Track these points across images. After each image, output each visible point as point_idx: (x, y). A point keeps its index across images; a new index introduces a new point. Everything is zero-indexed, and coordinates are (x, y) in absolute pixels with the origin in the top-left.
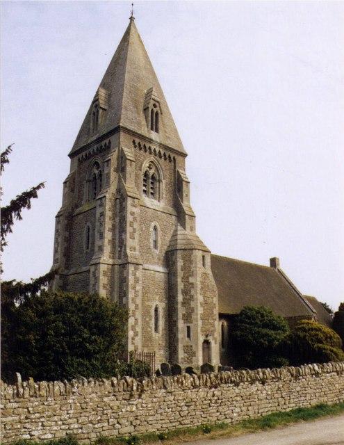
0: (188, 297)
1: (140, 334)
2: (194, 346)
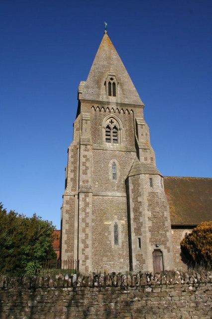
0: (138, 214)
1: (90, 246)
2: (143, 256)
